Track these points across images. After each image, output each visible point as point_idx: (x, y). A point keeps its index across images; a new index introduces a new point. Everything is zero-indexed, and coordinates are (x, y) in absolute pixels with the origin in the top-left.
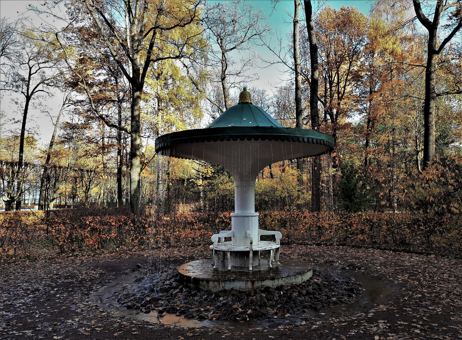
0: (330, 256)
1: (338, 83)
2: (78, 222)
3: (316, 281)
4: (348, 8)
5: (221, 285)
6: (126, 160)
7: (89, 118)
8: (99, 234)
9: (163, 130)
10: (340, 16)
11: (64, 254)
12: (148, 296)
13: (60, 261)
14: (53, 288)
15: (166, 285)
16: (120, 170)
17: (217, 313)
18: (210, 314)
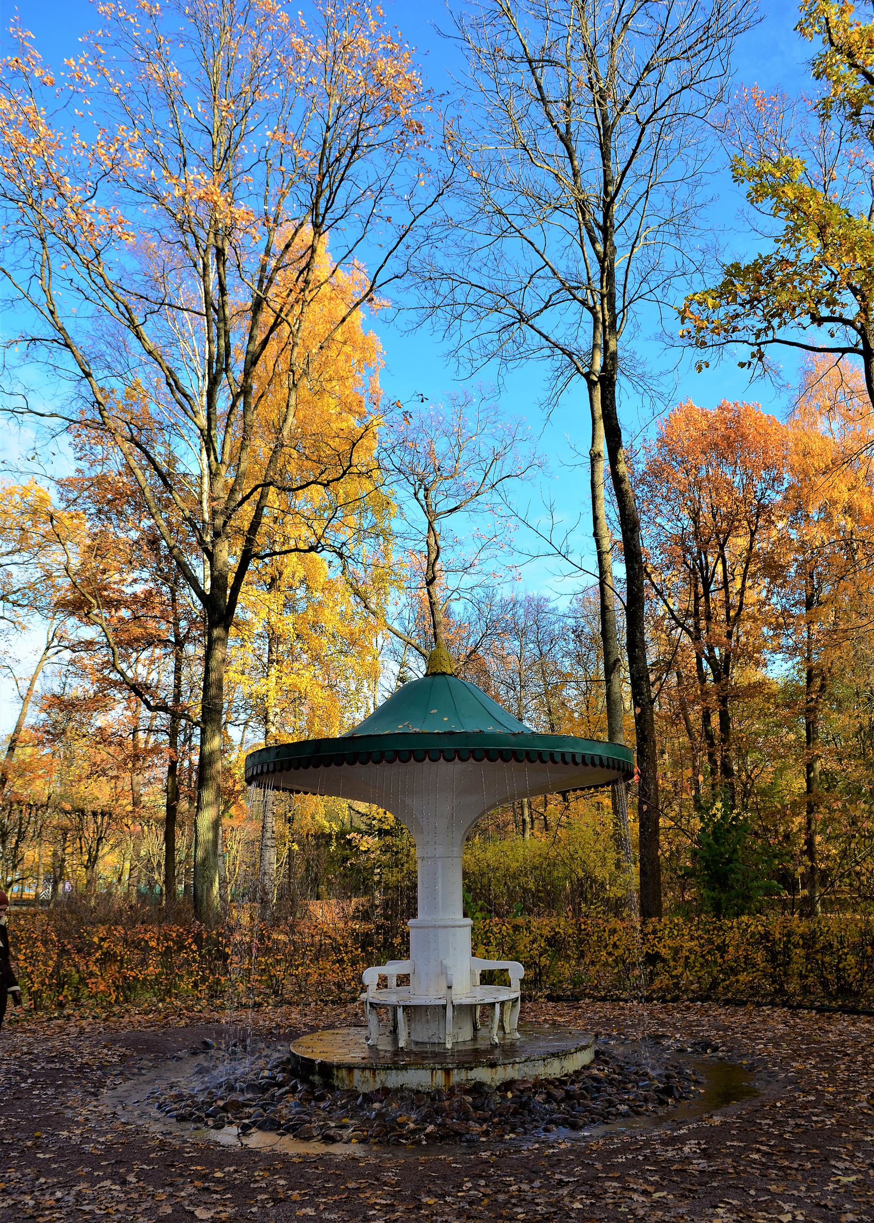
0: (662, 1024)
1: (726, 583)
2: (75, 939)
3: (596, 1072)
4: (736, 405)
5: (377, 1079)
6: (189, 786)
7: (106, 684)
8: (121, 967)
9: (278, 710)
10: (718, 424)
11: (41, 1013)
12: (222, 1099)
13: (33, 1027)
14: (25, 1079)
15: (262, 1078)
16: (171, 809)
17: (363, 1131)
18: (347, 1133)
